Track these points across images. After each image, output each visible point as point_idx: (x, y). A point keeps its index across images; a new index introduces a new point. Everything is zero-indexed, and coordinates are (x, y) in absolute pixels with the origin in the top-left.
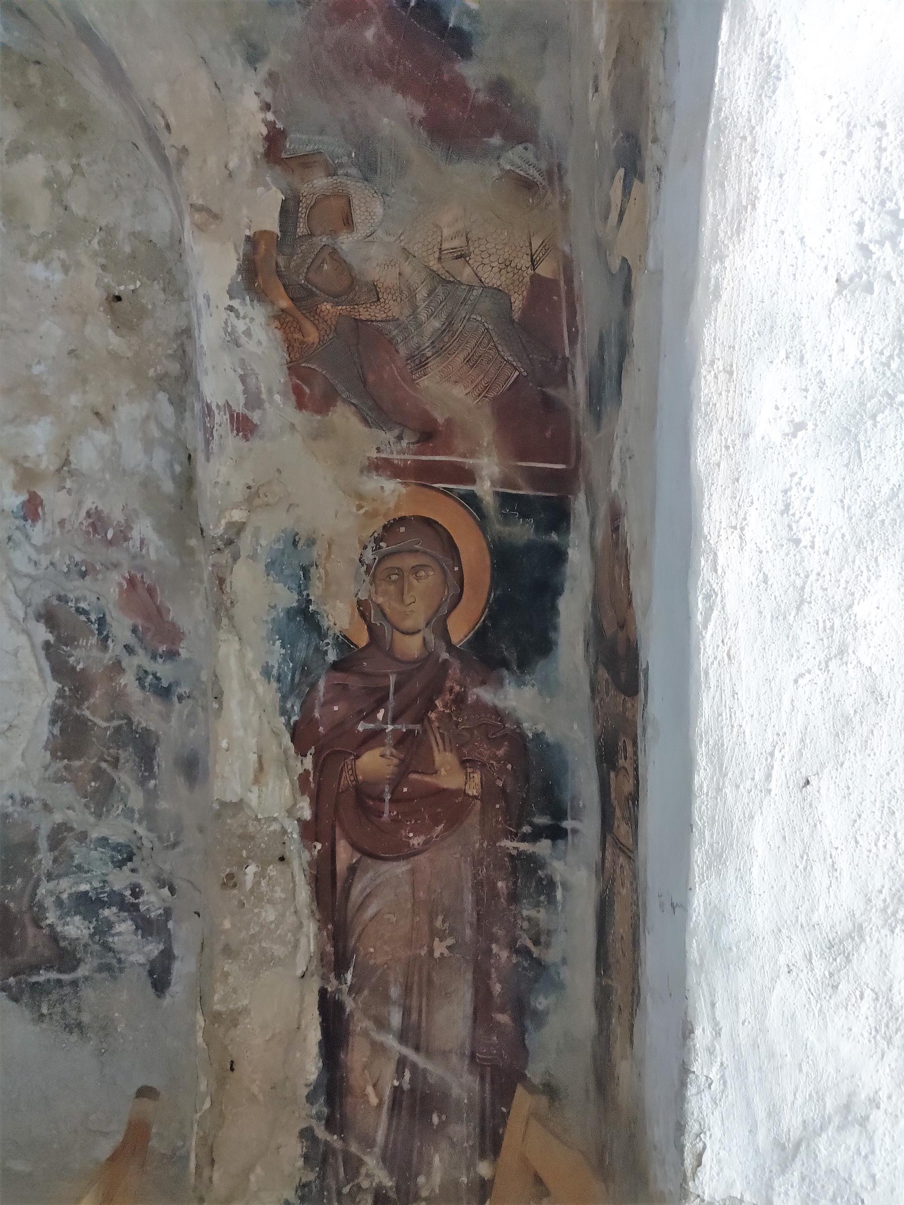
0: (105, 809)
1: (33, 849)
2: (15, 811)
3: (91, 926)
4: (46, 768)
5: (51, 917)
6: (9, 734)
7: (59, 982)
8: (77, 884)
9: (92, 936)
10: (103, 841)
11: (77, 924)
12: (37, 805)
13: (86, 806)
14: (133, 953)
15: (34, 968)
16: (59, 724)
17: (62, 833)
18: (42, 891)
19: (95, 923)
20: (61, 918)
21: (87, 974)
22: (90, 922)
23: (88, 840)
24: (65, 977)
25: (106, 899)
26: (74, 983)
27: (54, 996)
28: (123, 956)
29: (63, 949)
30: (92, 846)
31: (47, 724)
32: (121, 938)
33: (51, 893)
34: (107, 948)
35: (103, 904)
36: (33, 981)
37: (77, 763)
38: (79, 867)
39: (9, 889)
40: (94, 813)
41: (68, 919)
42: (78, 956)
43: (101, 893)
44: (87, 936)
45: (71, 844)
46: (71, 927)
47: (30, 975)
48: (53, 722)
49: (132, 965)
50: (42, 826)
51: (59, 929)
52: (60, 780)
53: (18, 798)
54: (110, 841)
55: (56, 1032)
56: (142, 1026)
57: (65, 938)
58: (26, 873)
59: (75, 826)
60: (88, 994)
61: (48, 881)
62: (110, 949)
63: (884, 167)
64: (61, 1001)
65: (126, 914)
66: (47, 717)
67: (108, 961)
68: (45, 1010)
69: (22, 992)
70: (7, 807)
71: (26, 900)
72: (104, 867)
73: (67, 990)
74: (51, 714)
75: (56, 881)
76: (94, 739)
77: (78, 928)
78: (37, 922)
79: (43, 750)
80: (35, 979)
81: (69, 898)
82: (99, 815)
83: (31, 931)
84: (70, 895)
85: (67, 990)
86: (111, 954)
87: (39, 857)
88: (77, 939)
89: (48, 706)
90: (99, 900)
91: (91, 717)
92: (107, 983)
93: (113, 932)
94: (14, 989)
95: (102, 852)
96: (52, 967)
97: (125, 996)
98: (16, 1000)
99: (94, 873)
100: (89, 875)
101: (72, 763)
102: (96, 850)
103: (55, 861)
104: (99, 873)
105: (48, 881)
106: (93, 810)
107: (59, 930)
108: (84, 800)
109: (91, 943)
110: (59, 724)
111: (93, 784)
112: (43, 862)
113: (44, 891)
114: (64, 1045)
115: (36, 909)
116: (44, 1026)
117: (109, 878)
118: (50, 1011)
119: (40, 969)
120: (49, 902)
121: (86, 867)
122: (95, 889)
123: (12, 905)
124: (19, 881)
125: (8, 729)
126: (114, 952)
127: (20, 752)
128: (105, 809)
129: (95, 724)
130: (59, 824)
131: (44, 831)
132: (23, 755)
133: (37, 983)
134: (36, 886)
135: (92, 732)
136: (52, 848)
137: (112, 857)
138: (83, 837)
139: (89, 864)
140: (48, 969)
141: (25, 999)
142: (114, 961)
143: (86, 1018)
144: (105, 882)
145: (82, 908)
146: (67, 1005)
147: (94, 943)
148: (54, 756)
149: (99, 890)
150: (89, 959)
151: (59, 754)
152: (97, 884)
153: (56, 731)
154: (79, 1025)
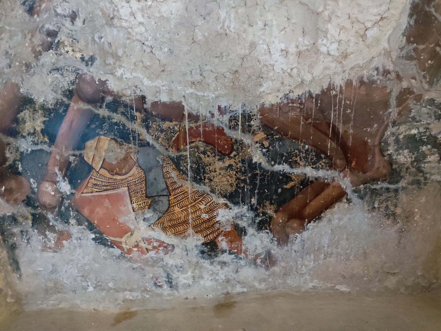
0: (435, 80)
1: (386, 105)
2: (378, 79)
3: (413, 156)
4: (402, 49)
5: (391, 150)
6: (380, 23)
7: (388, 189)
8: (410, 129)
9: (412, 163)
10: (432, 102)
11: (406, 155)
12: (393, 75)
13: (424, 77)
14: (434, 174)
15: (374, 180)
16: (415, 17)
17: (406, 95)
18: (388, 133)
19: (416, 154)
20: (397, 150)
21: (404, 185)
22: (413, 154)
23: (422, 101)
24: (392, 187)
25: (425, 140)
26: (396, 191)
27: (383, 198)
28: (428, 176)
29: (395, 170)
30: (424, 105)
31: (407, 16)
32: (429, 164)
33: (393, 134)
34: (419, 170)
35: (424, 143)
36: (374, 188)
37: (421, 47)
38: (414, 118)
39: (369, 130)
40: (429, 82)
41: (401, 151)
42: (402, 174)
43: (423, 136)
44: (410, 162)
45: (411, 103)
46: (401, 156)
47: (372, 184)
48: (411, 16)
49: (433, 181)
50: (394, 90)
51: (394, 157)
52: (409, 58)
53: (381, 70)
54: (436, 102)
55: (379, 217)
56: (429, 217)
57: (396, 163)
58: (380, 121)
59: (415, 90)
60: (403, 197)
61: (393, 127)
62: (422, 171)
63: (98, 79)
64: (387, 200)
65: (436, 150)
66: (408, 11)
67: (418, 178)
68: (376, 205)
69: (366, 194)
70: (374, 76)
71: (378, 138)
72: (429, 119)
73: (392, 194)
74: (411, 9)
75: (398, 127)
76: (434, 30)
77: (405, 157)
78: (382, 152)
79: (401, 36)
80: (374, 187)
81: (403, 138)
82: (431, 83)
83: (378, 157)
84: (405, 136)
85: (392, 194)
86: (421, 174)
87: (390, 110)
88: (404, 164)
89: (410, 3)
90: (421, 140)
91: (434, 13)
92: (415, 191)
93: (425, 161)
94: (362, 192)
95: (429, 109)
96: (385, 180)
97: (423, 200)
98: (362, 198)
99: (422, 123)
100: (419, 124)
101: (418, 46)
102: (426, 107)
103: (399, 114)
104: (425, 122)
105: (393, 127)
106: (428, 80)
107: (394, 158)
108: (423, 73)
109: (411, 167)
110: (415, 17)
111: (430, 62)
112: (391, 114)
113: (389, 133)
114: (382, 226)
115: (383, 144)
116: (374, 214)
117: (431, 126)
118: (379, 206)
119: (379, 180)
120: (391, 140)
121: (418, 118)
122: (420, 133)
123: (369, 141)
124: (375, 126)
125: (380, 20)
126: (423, 173)
127: (387, 37)
128: (435, 80)
129: (436, 19)
130: (405, 89)
131: (394, 94)
132: (389, 39)
133: (375, 189)
134: (386, 129)
135: (434, 24)
136: (398, 105)
137: (435, 112)
138: (419, 98)
139: (420, 117)
140: (383, 181)
141: (367, 198)
142: (422, 179)
143: (398, 211)
144: (427, 128)
145: (410, 145)
146: (389, 202)
147: (413, 167)
148: (409, 41)
149: (423, 134)
150: (407, 177)
151: (412, 39)
152: (422, 130)
153: (412, 23)
154: (394, 214)
